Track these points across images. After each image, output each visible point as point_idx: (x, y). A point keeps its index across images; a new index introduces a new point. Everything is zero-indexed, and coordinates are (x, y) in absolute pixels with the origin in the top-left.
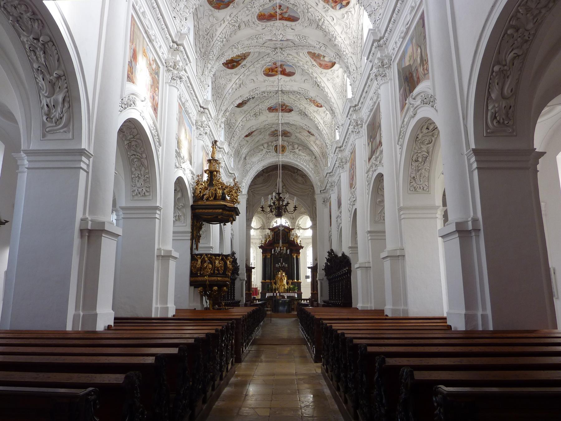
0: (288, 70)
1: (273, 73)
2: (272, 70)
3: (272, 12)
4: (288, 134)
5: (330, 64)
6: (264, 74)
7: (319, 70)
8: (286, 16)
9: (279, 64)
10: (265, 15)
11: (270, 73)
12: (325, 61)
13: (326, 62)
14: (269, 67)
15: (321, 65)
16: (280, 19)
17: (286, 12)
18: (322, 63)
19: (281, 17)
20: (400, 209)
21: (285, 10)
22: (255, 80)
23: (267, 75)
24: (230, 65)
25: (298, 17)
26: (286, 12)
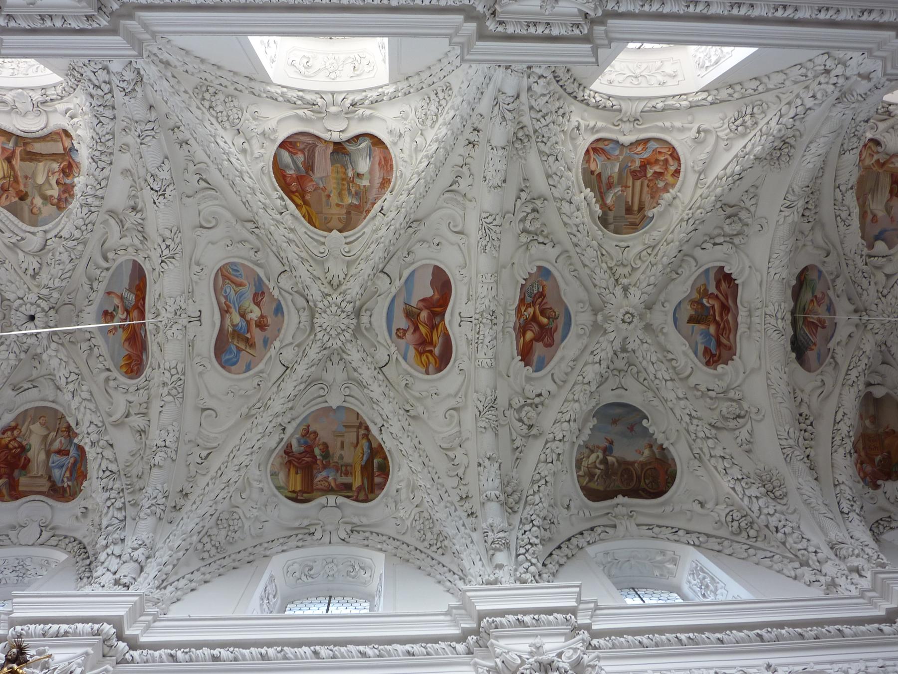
0: (424, 290)
1: (437, 339)
2: (423, 345)
3: (122, 335)
4: (539, 349)
5: (377, 151)
6: (439, 369)
7: (397, 182)
8: (132, 298)
9: (695, 296)
10: (129, 357)
11: (437, 351)
12: (371, 171)
13: (372, 165)
14: (412, 352)
15: (385, 183)
16: (142, 316)
17: (122, 298)
18: (377, 181)
19: (135, 313)
20: (568, 558)
21: (117, 301)
22: (452, 403)
23: (444, 359)
24: (377, 480)
25: (130, 265)
26: (122, 298)
